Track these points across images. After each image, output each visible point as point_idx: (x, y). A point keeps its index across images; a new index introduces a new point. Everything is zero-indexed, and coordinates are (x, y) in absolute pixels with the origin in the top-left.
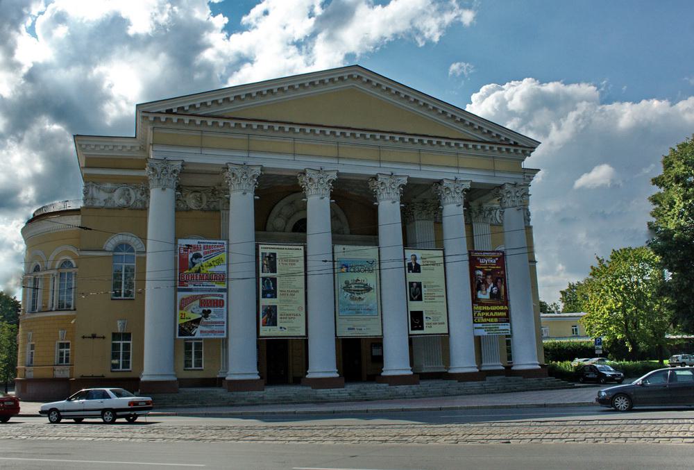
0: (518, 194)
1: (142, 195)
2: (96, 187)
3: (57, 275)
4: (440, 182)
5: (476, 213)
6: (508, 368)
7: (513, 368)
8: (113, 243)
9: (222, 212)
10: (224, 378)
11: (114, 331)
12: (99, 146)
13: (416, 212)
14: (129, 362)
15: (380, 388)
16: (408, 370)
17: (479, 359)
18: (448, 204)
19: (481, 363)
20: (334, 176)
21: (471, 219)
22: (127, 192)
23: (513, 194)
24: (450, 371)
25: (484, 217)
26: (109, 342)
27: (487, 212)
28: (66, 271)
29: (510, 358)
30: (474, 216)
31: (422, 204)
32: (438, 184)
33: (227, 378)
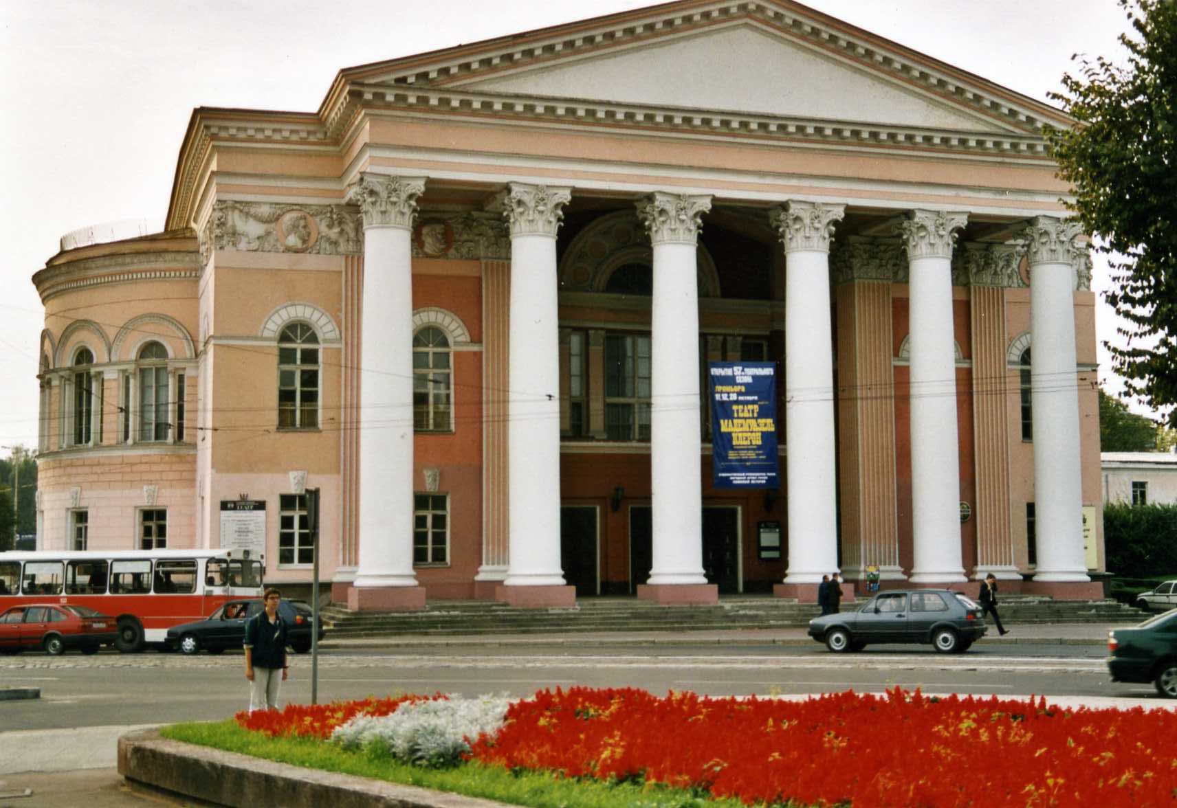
0: (1063, 238)
1: (330, 226)
2: (241, 211)
3: (135, 374)
4: (908, 214)
5: (978, 265)
6: (1028, 578)
7: (1036, 578)
8: (279, 322)
9: (483, 261)
10: (350, 584)
11: (322, 494)
12: (245, 129)
13: (856, 262)
14: (444, 550)
15: (542, 662)
16: (555, 575)
17: (970, 557)
18: (921, 257)
19: (976, 564)
20: (706, 205)
21: (968, 277)
22: (302, 223)
23: (1054, 236)
24: (915, 579)
25: (995, 273)
26: (274, 510)
27: (1001, 264)
28: (150, 362)
29: (1033, 558)
30: (974, 270)
31: (868, 247)
32: (903, 217)
33: (357, 583)
